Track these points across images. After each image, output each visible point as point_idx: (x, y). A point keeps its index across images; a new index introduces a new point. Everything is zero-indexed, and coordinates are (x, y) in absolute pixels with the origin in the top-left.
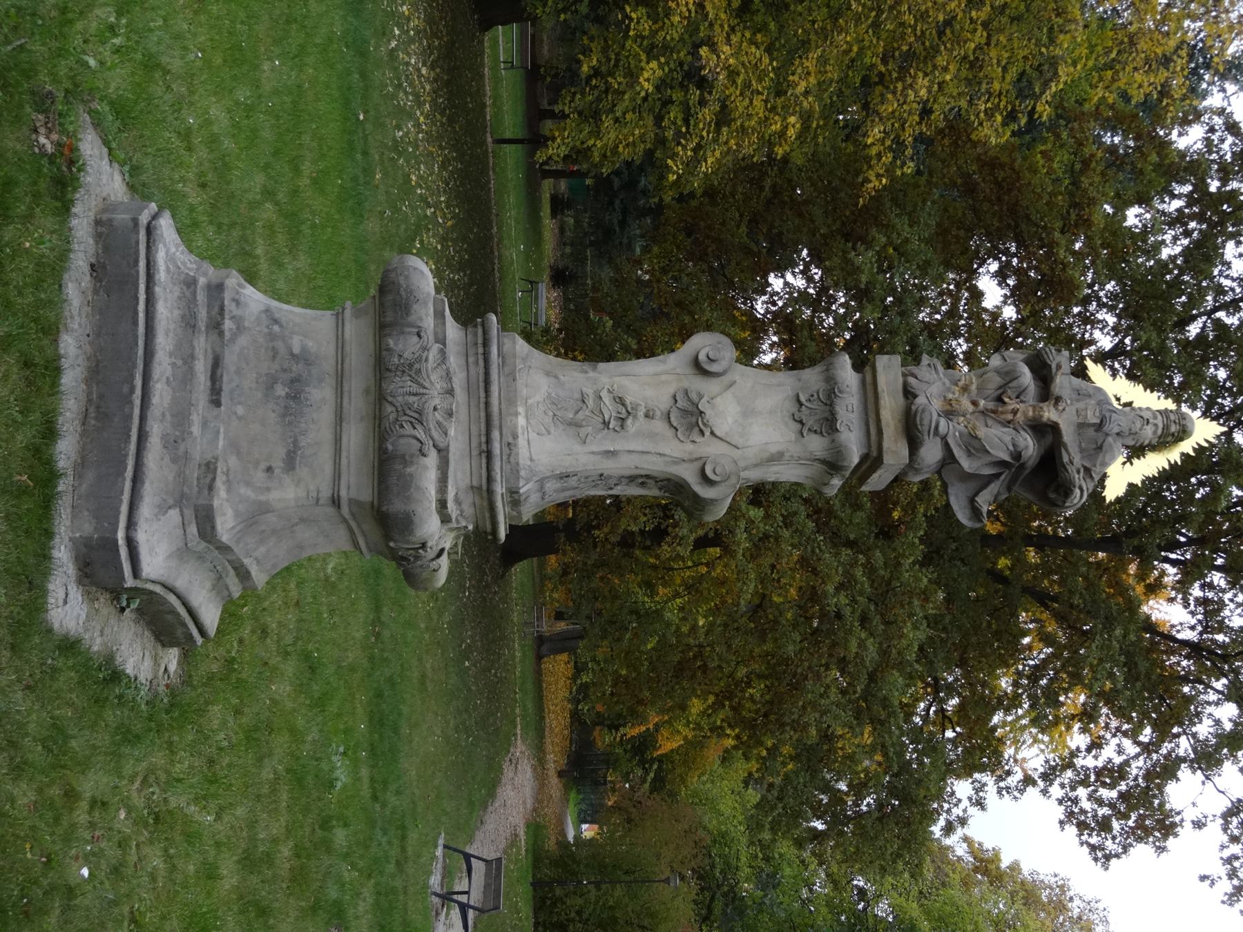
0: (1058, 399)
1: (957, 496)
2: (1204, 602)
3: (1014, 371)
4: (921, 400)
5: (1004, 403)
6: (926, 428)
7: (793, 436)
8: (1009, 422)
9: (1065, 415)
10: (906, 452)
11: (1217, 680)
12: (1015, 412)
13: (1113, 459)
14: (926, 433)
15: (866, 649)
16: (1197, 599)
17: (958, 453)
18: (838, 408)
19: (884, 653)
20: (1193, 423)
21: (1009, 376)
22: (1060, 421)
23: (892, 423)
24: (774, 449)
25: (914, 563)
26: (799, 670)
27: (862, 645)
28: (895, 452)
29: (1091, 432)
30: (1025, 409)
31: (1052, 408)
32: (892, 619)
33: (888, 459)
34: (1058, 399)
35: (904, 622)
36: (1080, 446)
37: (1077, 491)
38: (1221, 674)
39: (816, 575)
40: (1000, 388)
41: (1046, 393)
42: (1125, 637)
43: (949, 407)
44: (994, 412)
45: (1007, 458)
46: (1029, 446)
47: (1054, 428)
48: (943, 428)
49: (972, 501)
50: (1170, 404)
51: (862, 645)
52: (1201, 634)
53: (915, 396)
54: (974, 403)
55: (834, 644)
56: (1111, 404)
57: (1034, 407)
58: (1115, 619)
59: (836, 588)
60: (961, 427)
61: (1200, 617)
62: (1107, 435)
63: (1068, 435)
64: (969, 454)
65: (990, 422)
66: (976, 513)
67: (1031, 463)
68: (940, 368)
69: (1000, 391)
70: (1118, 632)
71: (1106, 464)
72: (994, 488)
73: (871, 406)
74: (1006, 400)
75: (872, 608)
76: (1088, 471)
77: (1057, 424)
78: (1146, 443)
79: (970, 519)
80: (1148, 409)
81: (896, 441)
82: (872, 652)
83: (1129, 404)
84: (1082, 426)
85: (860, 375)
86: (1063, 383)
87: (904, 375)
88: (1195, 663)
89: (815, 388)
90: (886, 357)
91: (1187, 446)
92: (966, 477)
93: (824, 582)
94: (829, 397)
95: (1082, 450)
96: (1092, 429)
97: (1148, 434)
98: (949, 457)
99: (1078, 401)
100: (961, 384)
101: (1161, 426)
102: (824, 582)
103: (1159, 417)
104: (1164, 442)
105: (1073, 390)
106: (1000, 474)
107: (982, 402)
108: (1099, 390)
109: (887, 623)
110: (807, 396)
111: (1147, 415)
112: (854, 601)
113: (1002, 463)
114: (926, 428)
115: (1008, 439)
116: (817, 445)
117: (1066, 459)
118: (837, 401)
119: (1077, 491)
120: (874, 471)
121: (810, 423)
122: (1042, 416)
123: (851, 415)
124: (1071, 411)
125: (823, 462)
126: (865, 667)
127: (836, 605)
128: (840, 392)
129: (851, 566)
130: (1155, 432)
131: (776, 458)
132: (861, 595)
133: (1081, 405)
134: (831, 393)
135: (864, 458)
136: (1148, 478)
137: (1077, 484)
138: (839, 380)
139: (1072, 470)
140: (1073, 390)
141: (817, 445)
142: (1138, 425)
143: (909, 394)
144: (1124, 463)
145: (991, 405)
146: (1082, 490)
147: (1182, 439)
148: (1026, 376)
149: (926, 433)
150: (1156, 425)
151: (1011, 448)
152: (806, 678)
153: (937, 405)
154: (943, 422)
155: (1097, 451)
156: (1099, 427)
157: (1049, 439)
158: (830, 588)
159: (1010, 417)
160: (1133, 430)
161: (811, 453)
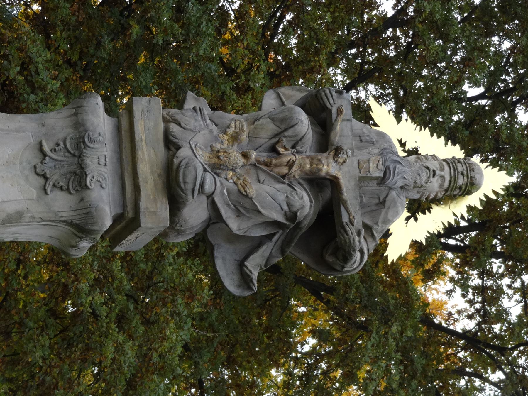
0: (338, 150)
1: (224, 259)
2: (481, 290)
3: (291, 118)
4: (184, 152)
5: (279, 154)
6: (190, 186)
7: (34, 193)
8: (284, 177)
9: (345, 168)
10: (166, 214)
11: (493, 372)
12: (290, 165)
13: (397, 215)
14: (189, 193)
15: (124, 353)
16: (475, 288)
17: (226, 213)
18: (88, 161)
19: (144, 358)
20: (481, 174)
21: (284, 124)
22: (340, 176)
23: (150, 179)
24: (11, 208)
25: (178, 255)
26: (48, 379)
27: (119, 348)
28: (154, 213)
29: (373, 186)
30: (302, 162)
31: (331, 161)
32: (152, 319)
33: (146, 221)
34: (338, 150)
35: (167, 322)
36: (361, 202)
37: (358, 255)
38: (497, 366)
39: (68, 270)
40: (275, 136)
41: (325, 143)
42: (401, 334)
43: (216, 160)
44: (266, 164)
45: (280, 218)
46: (305, 203)
47: (333, 183)
48: (209, 187)
49: (241, 265)
50: (456, 152)
51: (119, 348)
52: (479, 324)
53: (178, 148)
54: (245, 156)
55: (88, 349)
56: (396, 154)
57: (312, 159)
58: (391, 314)
59: (91, 286)
60: (230, 184)
61: (478, 306)
62: (390, 189)
63: (348, 191)
64: (239, 214)
65: (262, 177)
66: (245, 279)
67: (306, 223)
68: (207, 111)
69: (275, 140)
70: (395, 329)
71: (388, 222)
72: (265, 250)
73: (126, 153)
74: (281, 150)
75: (132, 307)
76: (368, 228)
77: (336, 178)
78: (432, 196)
79: (239, 286)
80: (433, 156)
81: (155, 200)
82: (130, 356)
83: (415, 152)
84: (363, 180)
85: (115, 119)
86: (344, 129)
87: (166, 121)
88: (471, 354)
89: (61, 135)
90: (144, 100)
91: (474, 200)
92: (233, 238)
93: (77, 279)
94: (77, 147)
95: (362, 206)
96: (375, 182)
97: (434, 186)
98: (215, 217)
99: (360, 149)
100: (230, 131)
101: (447, 178)
102: (77, 279)
103: (446, 168)
104: (450, 195)
105: (355, 136)
106: (274, 235)
107: (254, 155)
108: (383, 136)
109: (147, 322)
110: (52, 145)
111: (433, 165)
112: (111, 299)
113: (275, 224)
114: (190, 186)
115: (281, 198)
116: (62, 203)
117: (345, 219)
118: (87, 152)
119: (358, 255)
120: (130, 233)
121: (55, 177)
122: (320, 170)
123: (103, 169)
124: (352, 163)
125: (71, 224)
126: (123, 373)
127: (91, 305)
128: (91, 141)
129: (109, 260)
130: (441, 186)
131: (16, 218)
132: (120, 293)
133: (363, 155)
134: (80, 142)
135: (117, 219)
136: (432, 235)
137: (357, 248)
138: (89, 125)
139: (352, 231)
140: (355, 136)
141: (62, 203)
142: (424, 177)
143: (170, 144)
144: (408, 219)
145: (264, 156)
146: (362, 252)
147: (469, 193)
148: (304, 122)
149: (189, 193)
150: (442, 177)
151: (286, 208)
152: (56, 387)
153: (203, 157)
154: (209, 178)
155: (380, 206)
156: (382, 181)
157: (328, 193)
158: (84, 286)
159: (285, 170)
160: (419, 183)
161: (56, 213)
